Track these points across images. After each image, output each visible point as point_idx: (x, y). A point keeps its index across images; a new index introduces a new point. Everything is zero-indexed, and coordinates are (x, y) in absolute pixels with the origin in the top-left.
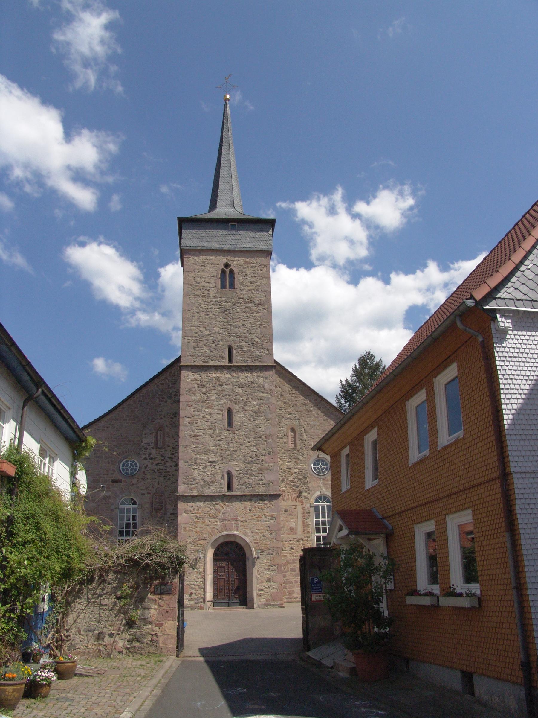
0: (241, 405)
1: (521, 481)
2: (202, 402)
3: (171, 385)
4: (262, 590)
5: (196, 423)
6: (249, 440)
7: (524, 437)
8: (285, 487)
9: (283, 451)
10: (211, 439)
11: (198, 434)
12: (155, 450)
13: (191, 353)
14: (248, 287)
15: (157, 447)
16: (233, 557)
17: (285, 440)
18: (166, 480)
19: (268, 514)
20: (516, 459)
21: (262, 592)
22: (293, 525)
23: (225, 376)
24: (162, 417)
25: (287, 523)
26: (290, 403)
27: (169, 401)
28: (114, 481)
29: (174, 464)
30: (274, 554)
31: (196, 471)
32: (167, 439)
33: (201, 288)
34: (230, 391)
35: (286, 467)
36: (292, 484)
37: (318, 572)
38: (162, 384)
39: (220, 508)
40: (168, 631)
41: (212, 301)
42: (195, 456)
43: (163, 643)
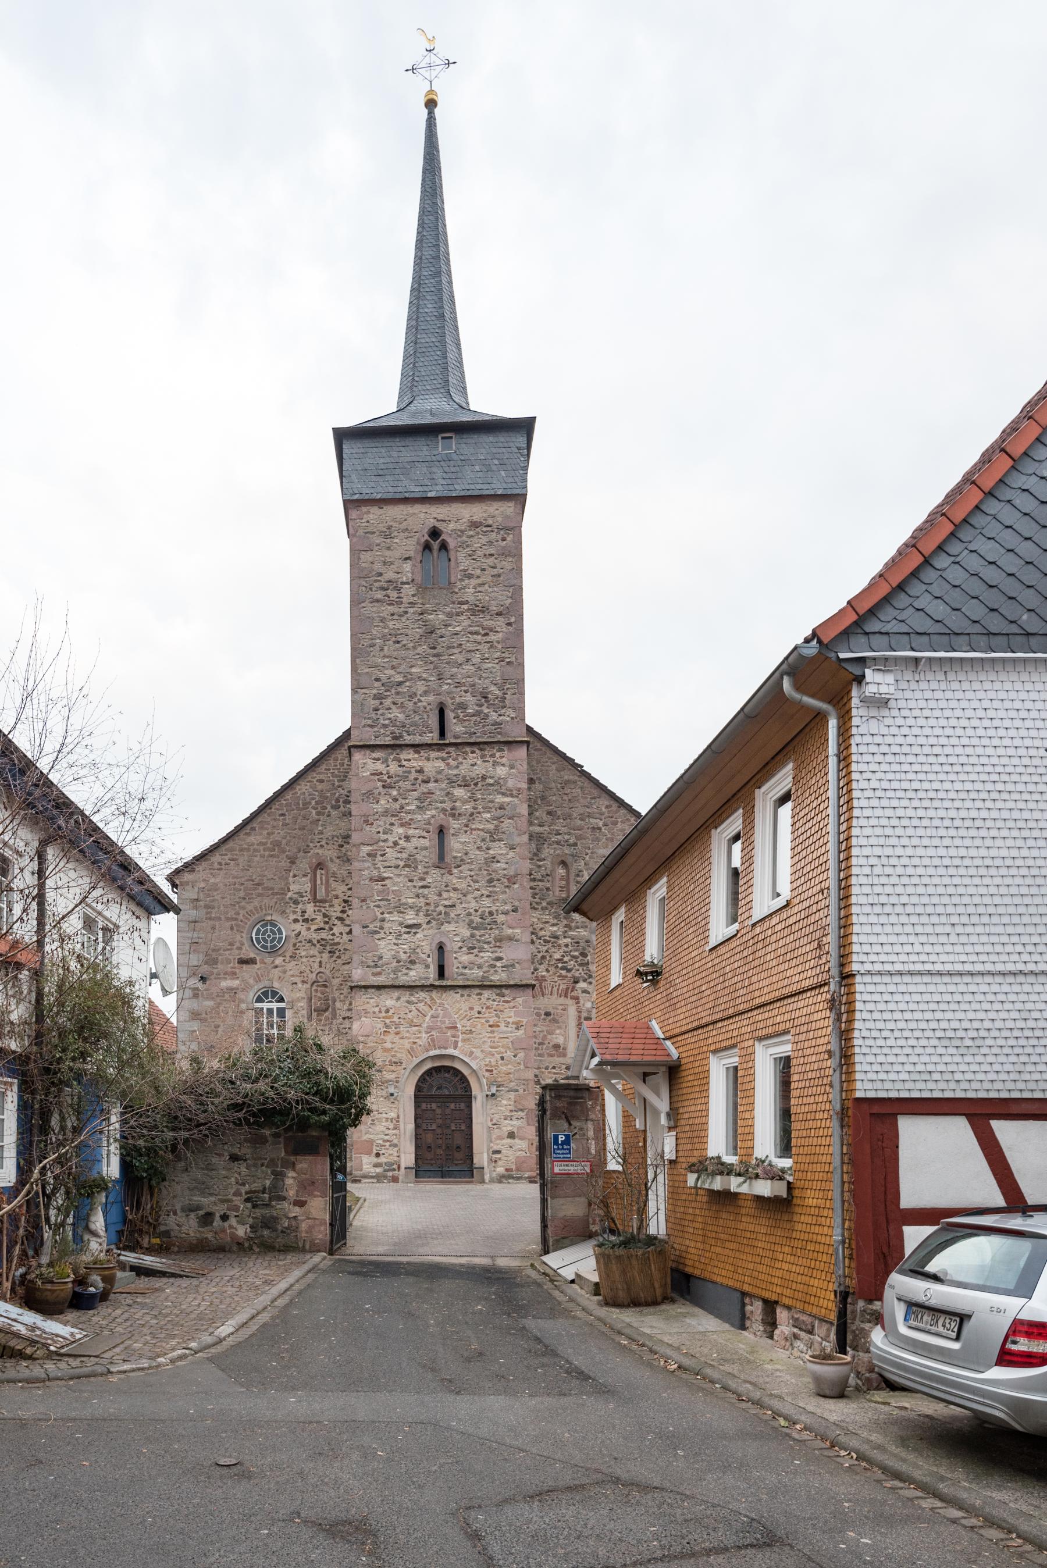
0: (463, 820)
1: (871, 988)
2: (393, 816)
3: (337, 784)
4: (499, 1152)
5: (382, 855)
6: (477, 886)
7: (888, 909)
8: (548, 971)
9: (544, 904)
10: (410, 884)
11: (385, 875)
12: (312, 904)
13: (369, 722)
14: (478, 577)
15: (315, 900)
16: (444, 1093)
17: (548, 885)
18: (334, 958)
19: (510, 1020)
20: (866, 948)
21: (498, 1156)
22: (560, 1040)
23: (432, 764)
24: (323, 843)
25: (549, 1037)
26: (559, 813)
27: (334, 813)
28: (243, 962)
29: (347, 929)
30: (521, 1091)
31: (382, 943)
32: (334, 885)
33: (386, 585)
34: (443, 793)
35: (548, 934)
36: (560, 965)
37: (566, 1125)
38: (321, 781)
39: (426, 1008)
40: (314, 1213)
41: (406, 612)
42: (380, 916)
43: (307, 1232)
